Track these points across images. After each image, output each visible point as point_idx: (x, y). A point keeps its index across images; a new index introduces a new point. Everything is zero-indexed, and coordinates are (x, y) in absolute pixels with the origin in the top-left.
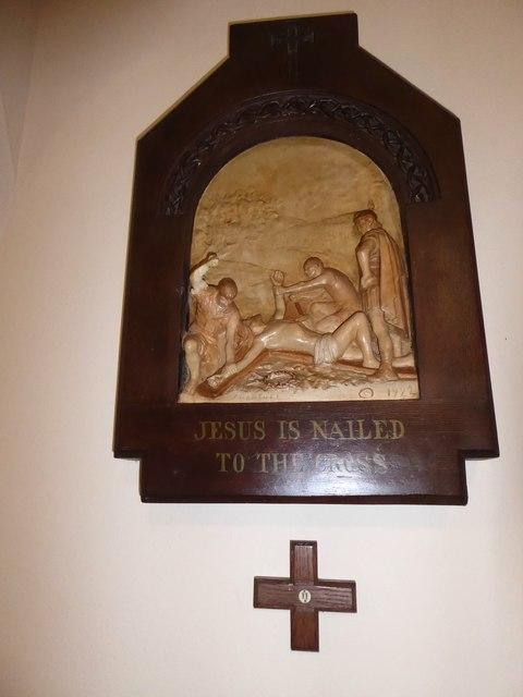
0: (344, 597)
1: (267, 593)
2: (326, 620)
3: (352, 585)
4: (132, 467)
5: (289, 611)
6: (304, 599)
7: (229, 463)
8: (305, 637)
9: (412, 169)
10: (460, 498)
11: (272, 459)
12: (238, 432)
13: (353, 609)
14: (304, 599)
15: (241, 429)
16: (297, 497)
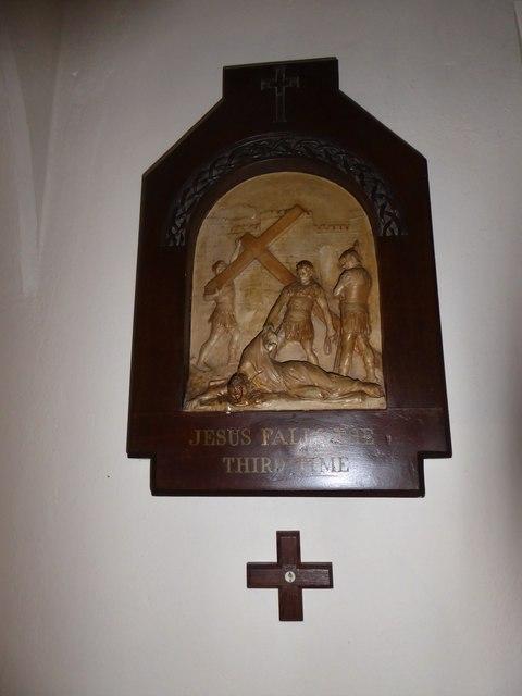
0: (322, 576)
1: (257, 576)
3: (329, 566)
5: (276, 591)
6: (289, 577)
7: (234, 465)
8: (291, 610)
9: (383, 206)
12: (228, 439)
14: (289, 577)
15: (231, 437)
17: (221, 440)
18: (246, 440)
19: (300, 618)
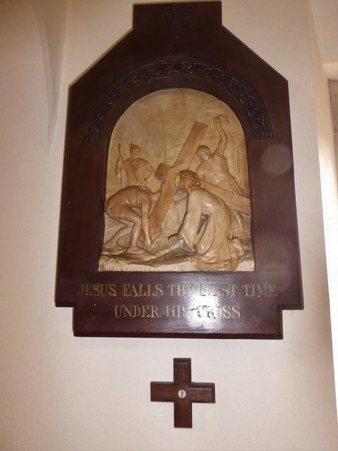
0: (207, 393)
1: (159, 392)
2: (197, 408)
4: (69, 311)
5: (173, 403)
6: (182, 394)
8: (183, 419)
10: (279, 336)
11: (151, 309)
13: (213, 401)
14: (182, 394)
16: (168, 334)
17: (97, 293)
18: (113, 293)
19: (190, 426)
